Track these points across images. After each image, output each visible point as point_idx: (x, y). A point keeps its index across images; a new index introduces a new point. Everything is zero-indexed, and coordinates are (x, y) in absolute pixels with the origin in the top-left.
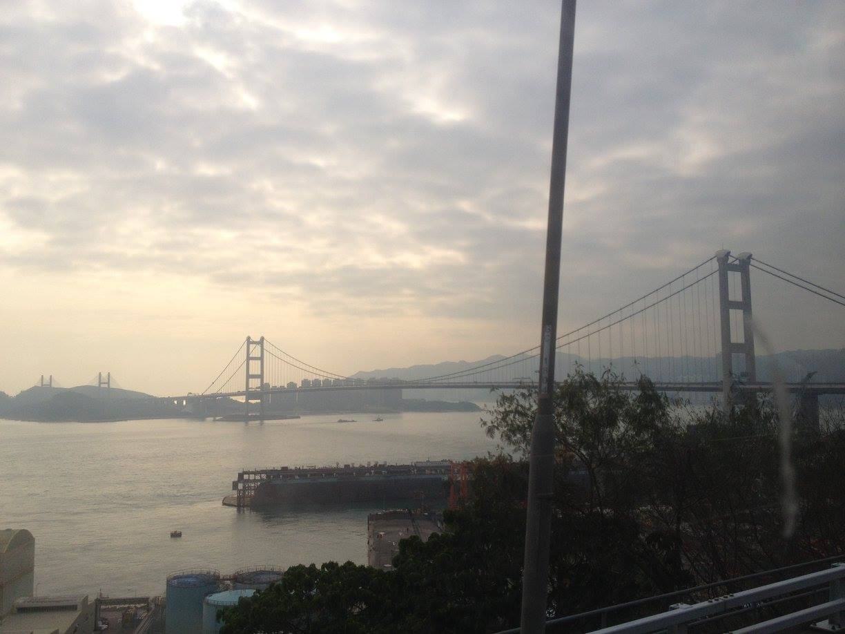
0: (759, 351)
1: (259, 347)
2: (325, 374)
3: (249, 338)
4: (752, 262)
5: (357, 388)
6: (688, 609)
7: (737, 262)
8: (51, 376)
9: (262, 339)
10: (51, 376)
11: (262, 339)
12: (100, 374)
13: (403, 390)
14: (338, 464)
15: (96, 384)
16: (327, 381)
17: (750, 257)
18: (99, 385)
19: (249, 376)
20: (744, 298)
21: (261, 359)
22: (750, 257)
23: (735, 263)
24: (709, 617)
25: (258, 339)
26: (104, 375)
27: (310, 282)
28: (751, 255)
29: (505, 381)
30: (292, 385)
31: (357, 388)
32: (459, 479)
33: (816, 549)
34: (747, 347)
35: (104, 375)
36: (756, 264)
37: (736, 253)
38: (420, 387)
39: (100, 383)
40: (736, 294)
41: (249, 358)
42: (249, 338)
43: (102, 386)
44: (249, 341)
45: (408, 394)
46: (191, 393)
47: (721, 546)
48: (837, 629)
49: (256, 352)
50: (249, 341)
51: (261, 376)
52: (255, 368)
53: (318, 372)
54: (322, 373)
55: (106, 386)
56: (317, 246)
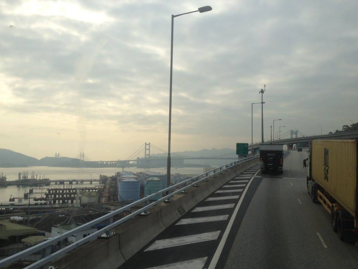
1: (148, 146)
4: (298, 132)
6: (52, 239)
8: (59, 153)
9: (150, 143)
10: (59, 153)
11: (150, 143)
12: (56, 153)
13: (184, 160)
15: (55, 157)
18: (145, 156)
19: (146, 155)
26: (57, 154)
27: (123, 120)
33: (53, 222)
35: (57, 154)
36: (299, 133)
37: (294, 130)
38: (207, 159)
39: (56, 156)
43: (57, 157)
45: (186, 162)
48: (108, 236)
49: (148, 147)
56: (125, 106)
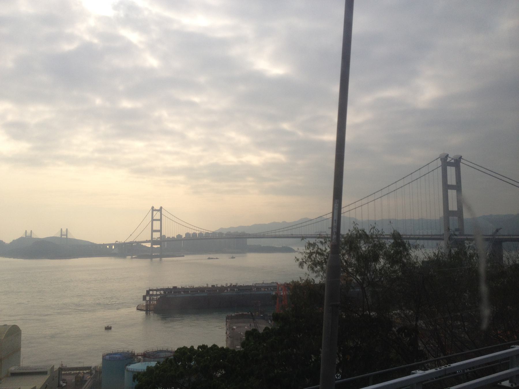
0: (466, 215)
2: (200, 230)
3: (153, 207)
4: (462, 161)
7: (453, 161)
9: (161, 208)
14: (207, 285)
17: (461, 158)
19: (153, 231)
20: (457, 183)
21: (160, 220)
25: (158, 208)
30: (179, 236)
40: (452, 180)
41: (153, 220)
42: (153, 207)
43: (63, 237)
44: (153, 209)
46: (117, 241)
50: (153, 209)
51: (160, 231)
53: (196, 228)
54: (198, 229)
55: (65, 237)
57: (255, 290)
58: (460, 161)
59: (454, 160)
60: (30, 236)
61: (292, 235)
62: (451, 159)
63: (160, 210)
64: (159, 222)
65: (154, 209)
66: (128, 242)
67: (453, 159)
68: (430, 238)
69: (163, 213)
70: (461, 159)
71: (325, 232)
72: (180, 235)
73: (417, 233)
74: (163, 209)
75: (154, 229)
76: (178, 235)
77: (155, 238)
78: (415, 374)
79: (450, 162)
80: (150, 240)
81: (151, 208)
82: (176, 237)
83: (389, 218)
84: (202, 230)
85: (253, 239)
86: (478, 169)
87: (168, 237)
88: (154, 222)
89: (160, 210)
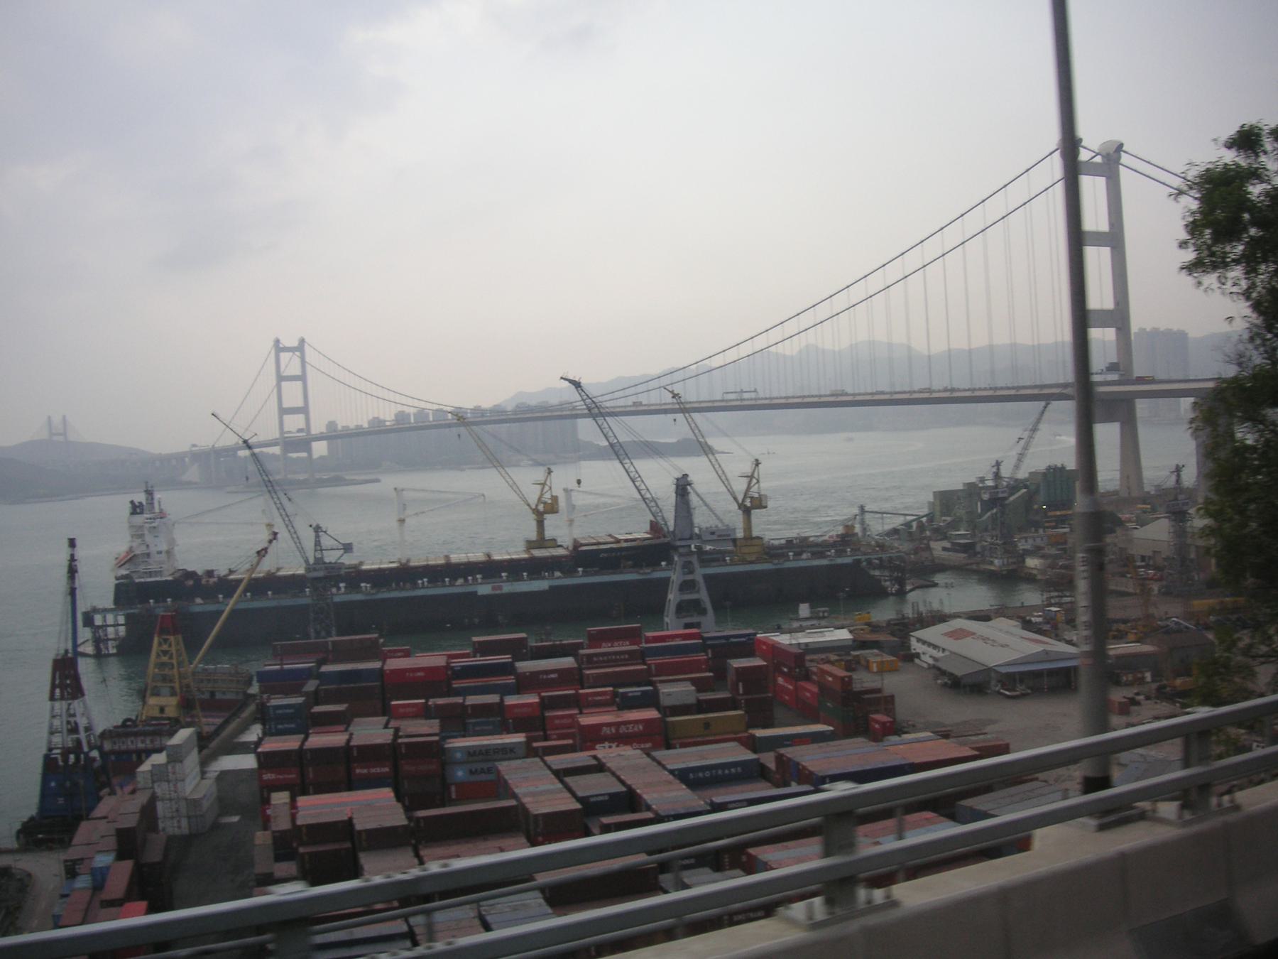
0: (1140, 320)
2: (416, 403)
3: (277, 341)
4: (1125, 159)
5: (436, 427)
7: (1098, 159)
9: (302, 341)
11: (302, 341)
14: (408, 561)
16: (421, 413)
17: (1120, 148)
19: (283, 411)
20: (1111, 225)
21: (302, 378)
22: (1120, 148)
23: (1095, 160)
24: (144, 726)
25: (294, 343)
28: (1121, 145)
29: (783, 395)
30: (377, 421)
31: (436, 427)
32: (547, 574)
34: (1119, 317)
40: (1095, 218)
41: (281, 378)
42: (277, 341)
43: (55, 438)
44: (279, 348)
46: (194, 446)
47: (100, 631)
50: (279, 348)
51: (304, 410)
52: (292, 393)
53: (404, 400)
54: (410, 402)
55: (61, 438)
57: (426, 584)
58: (1119, 158)
59: (1103, 156)
60: (61, 434)
61: (930, 391)
62: (1094, 154)
63: (300, 347)
64: (299, 383)
65: (281, 346)
66: (221, 445)
67: (1097, 154)
68: (948, 398)
69: (307, 359)
70: (1122, 154)
71: (755, 391)
72: (378, 418)
73: (937, 385)
74: (306, 346)
75: (285, 405)
76: (374, 418)
77: (290, 432)
78: (827, 791)
79: (1092, 163)
80: (277, 439)
81: (272, 343)
82: (366, 425)
83: (1036, 343)
84: (423, 405)
85: (663, 416)
86: (1162, 181)
87: (343, 427)
88: (284, 384)
89: (300, 347)
